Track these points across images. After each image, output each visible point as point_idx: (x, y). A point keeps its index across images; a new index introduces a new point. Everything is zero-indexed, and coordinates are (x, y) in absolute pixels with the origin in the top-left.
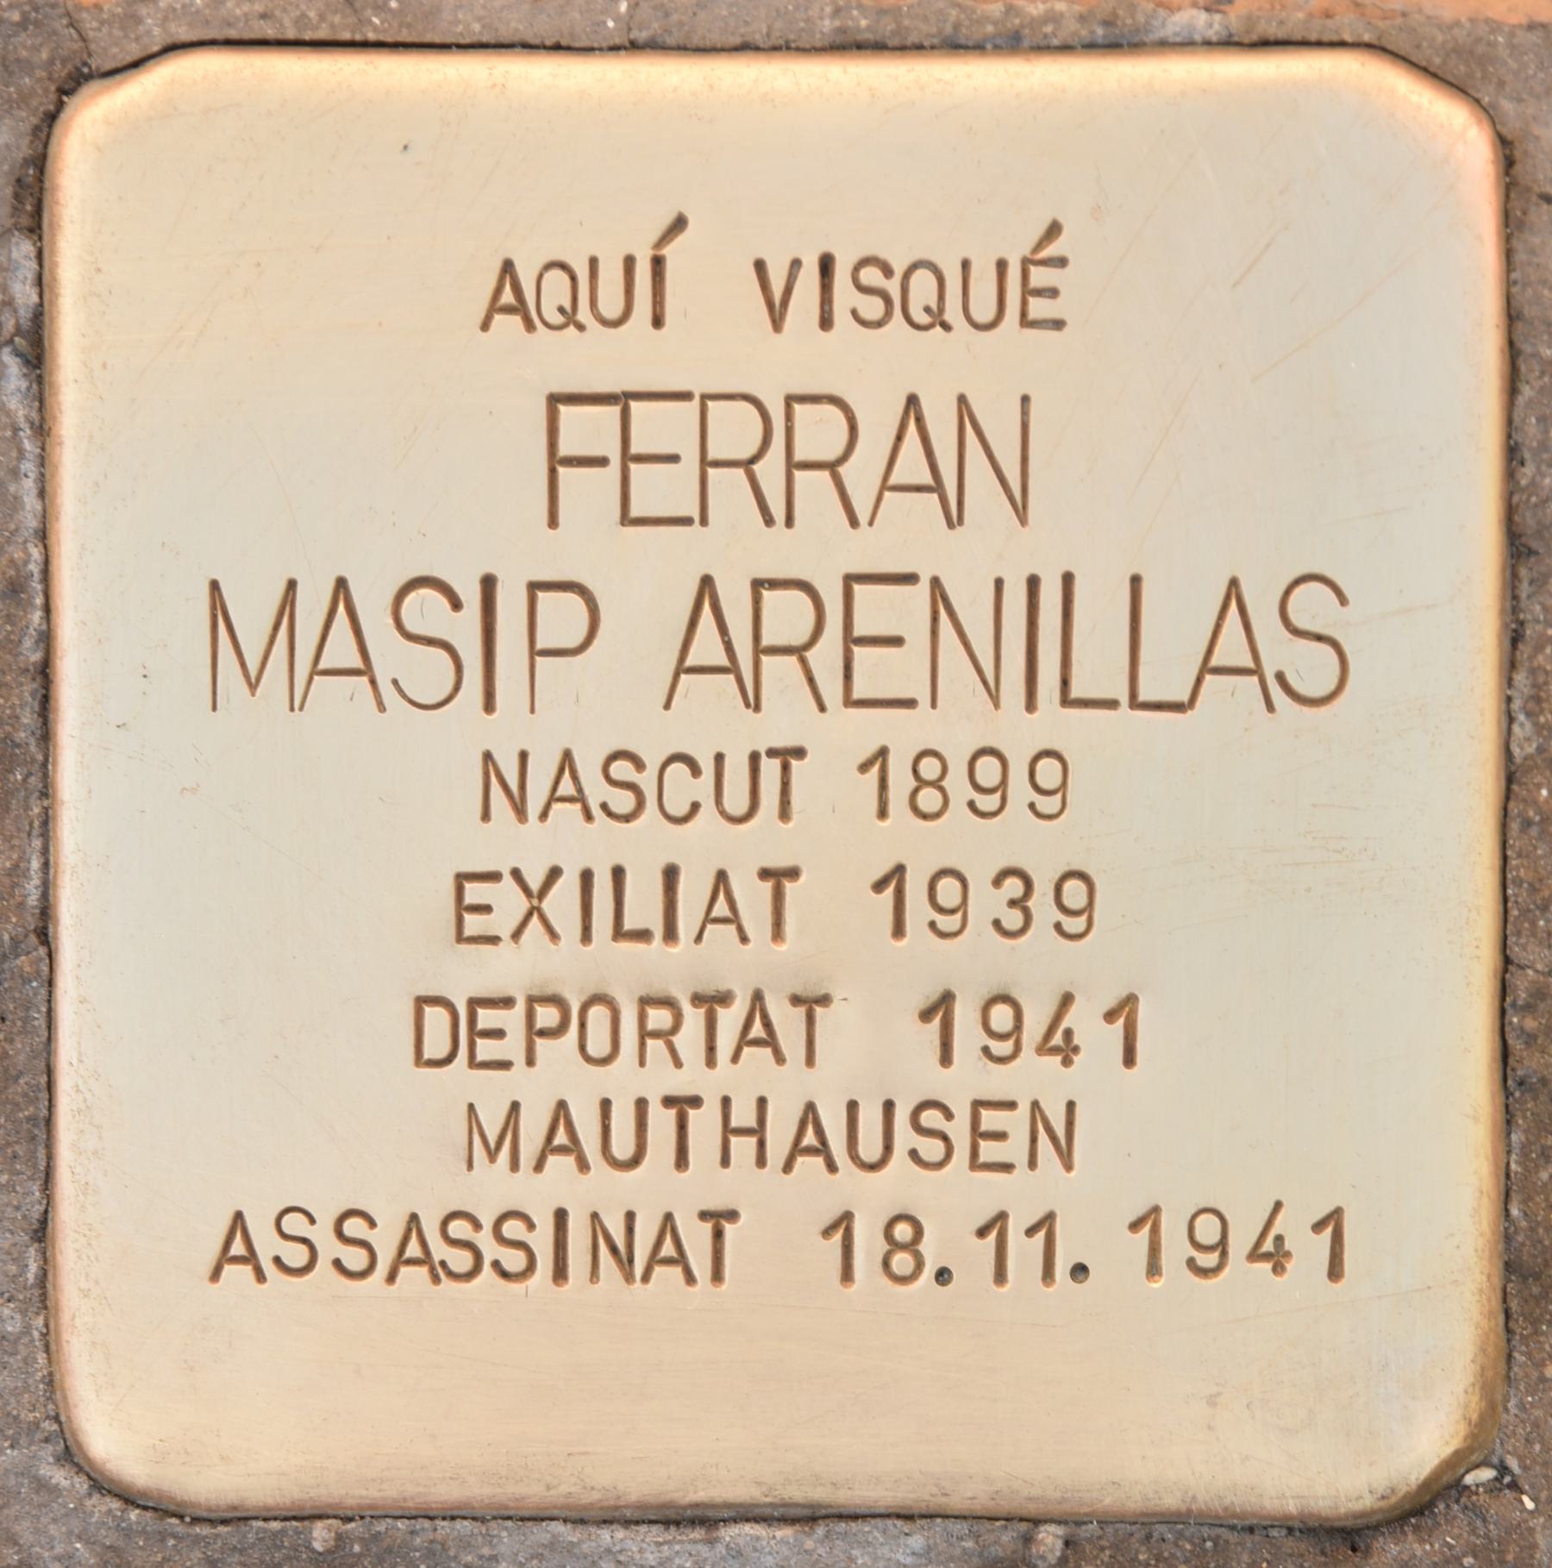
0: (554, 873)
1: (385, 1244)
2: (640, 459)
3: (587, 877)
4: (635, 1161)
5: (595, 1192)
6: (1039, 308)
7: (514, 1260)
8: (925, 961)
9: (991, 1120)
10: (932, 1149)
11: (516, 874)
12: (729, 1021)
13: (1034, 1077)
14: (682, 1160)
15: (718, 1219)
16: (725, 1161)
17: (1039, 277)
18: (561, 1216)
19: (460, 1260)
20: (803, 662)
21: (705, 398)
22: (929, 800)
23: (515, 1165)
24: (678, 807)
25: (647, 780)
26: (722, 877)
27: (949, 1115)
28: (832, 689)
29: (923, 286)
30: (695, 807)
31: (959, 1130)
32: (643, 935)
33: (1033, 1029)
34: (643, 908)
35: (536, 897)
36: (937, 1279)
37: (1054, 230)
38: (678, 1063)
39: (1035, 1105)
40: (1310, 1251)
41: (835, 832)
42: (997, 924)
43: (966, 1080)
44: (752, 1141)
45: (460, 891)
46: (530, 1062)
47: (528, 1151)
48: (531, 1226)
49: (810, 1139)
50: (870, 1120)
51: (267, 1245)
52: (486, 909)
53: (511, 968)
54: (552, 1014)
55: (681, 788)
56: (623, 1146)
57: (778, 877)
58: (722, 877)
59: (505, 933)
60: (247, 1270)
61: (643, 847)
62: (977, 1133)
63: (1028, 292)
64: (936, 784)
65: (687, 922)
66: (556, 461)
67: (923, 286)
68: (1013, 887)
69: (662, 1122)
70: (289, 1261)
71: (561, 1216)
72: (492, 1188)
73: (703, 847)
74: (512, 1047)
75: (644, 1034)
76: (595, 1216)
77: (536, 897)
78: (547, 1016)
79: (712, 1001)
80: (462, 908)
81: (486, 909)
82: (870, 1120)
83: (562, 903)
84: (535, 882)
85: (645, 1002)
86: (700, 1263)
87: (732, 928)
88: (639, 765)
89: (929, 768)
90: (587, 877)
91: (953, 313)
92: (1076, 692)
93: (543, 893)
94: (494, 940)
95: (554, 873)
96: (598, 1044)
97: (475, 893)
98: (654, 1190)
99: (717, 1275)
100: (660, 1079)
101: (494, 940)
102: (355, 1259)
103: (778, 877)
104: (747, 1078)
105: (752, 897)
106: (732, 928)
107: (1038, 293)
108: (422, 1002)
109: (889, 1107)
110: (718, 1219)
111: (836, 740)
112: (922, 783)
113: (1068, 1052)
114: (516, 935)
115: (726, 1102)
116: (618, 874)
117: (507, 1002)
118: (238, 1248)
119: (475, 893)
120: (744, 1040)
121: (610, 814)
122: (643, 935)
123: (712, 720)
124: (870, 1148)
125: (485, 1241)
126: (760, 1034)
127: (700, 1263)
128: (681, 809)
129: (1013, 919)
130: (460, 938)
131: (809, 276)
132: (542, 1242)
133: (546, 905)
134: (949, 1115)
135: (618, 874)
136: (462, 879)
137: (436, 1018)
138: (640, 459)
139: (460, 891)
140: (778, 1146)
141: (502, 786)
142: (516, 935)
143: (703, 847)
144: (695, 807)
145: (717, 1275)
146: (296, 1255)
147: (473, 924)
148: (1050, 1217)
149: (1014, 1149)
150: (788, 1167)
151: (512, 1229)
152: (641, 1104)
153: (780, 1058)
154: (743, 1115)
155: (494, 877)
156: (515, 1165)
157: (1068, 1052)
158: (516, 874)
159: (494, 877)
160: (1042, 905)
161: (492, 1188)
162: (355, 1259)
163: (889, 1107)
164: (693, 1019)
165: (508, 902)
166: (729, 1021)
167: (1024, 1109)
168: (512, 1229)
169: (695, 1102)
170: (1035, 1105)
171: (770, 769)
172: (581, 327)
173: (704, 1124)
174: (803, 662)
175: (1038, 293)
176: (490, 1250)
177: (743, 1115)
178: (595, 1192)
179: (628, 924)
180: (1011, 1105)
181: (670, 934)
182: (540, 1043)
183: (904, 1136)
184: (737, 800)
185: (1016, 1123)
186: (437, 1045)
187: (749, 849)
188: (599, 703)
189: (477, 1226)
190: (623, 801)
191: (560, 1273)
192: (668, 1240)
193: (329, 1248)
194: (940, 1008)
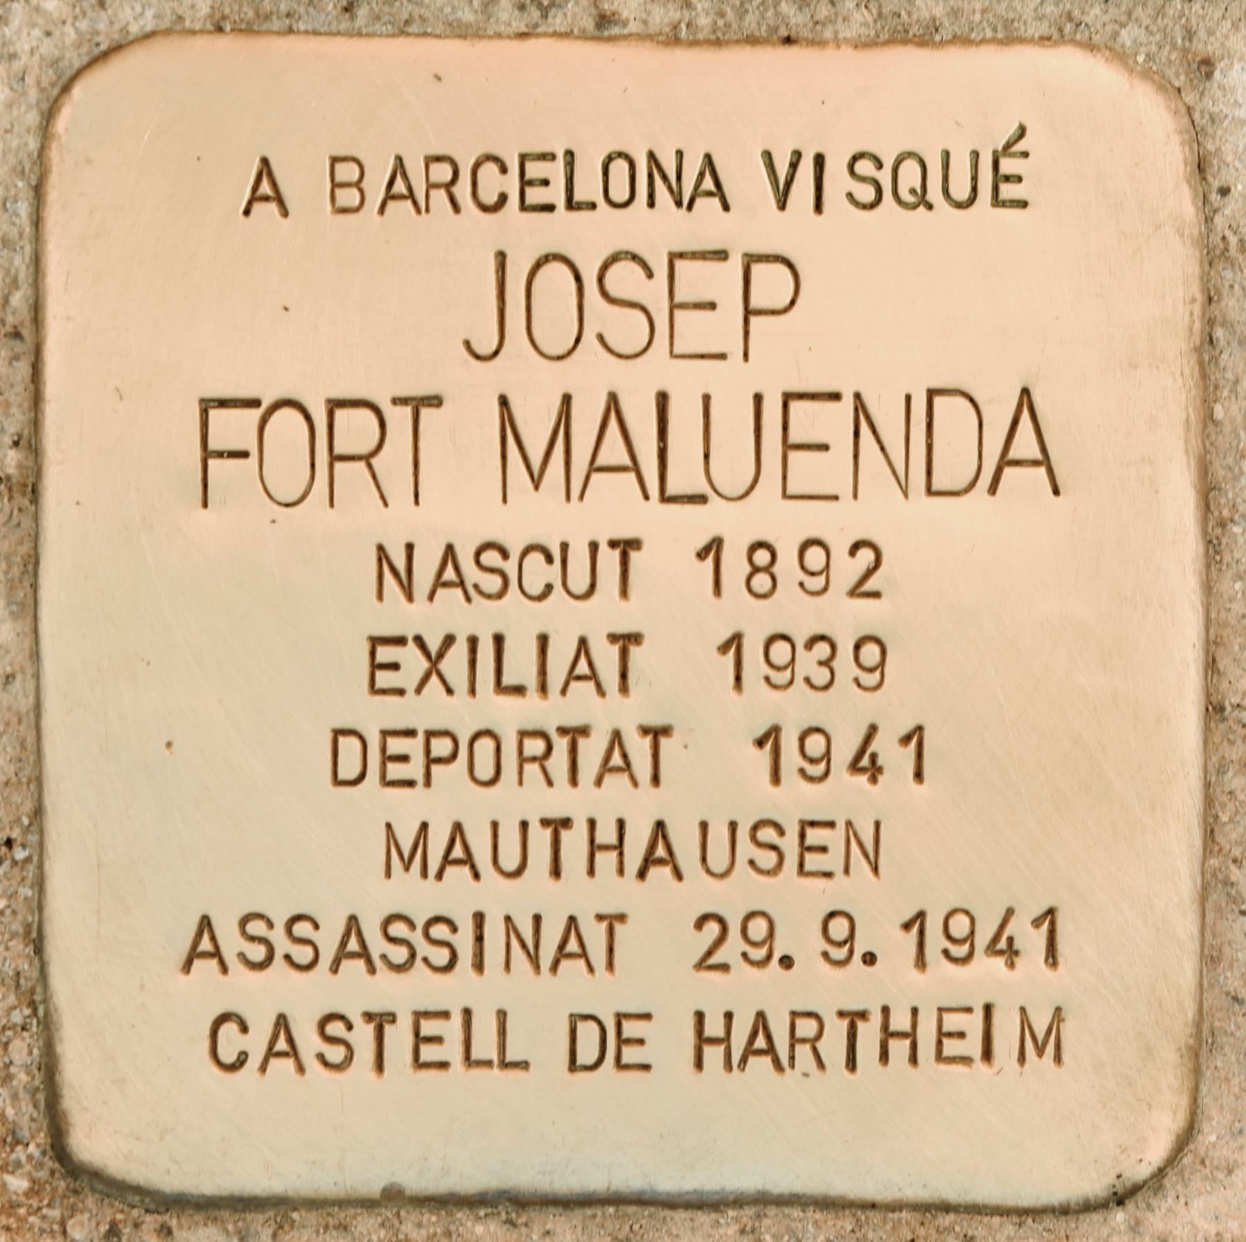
0: (449, 640)
1: (328, 943)
2: (683, 306)
3: (473, 642)
4: (518, 872)
5: (496, 897)
6: (1007, 191)
7: (440, 956)
8: (762, 705)
9: (815, 836)
10: (767, 859)
11: (419, 640)
12: (592, 751)
13: (844, 794)
14: (556, 872)
15: (613, 920)
16: (591, 871)
17: (1007, 166)
18: (479, 919)
19: (399, 954)
20: (370, 466)
21: (751, 260)
22: (762, 582)
23: (424, 874)
24: (536, 588)
25: (511, 567)
26: (583, 642)
27: (781, 832)
28: (653, 489)
29: (910, 175)
30: (549, 588)
31: (790, 844)
32: (519, 690)
33: (843, 752)
34: (520, 667)
35: (434, 661)
36: (865, 962)
37: (1022, 132)
38: (550, 783)
39: (849, 824)
40: (1032, 941)
41: (674, 604)
42: (807, 680)
43: (796, 799)
44: (614, 855)
45: (373, 654)
46: (428, 783)
47: (433, 867)
48: (454, 929)
49: (659, 852)
50: (718, 835)
51: (231, 943)
52: (395, 666)
53: (430, 708)
54: (441, 749)
55: (538, 573)
56: (510, 861)
57: (626, 641)
58: (583, 642)
59: (411, 688)
60: (360, 964)
61: (518, 620)
62: (805, 849)
63: (1000, 178)
64: (767, 569)
65: (557, 675)
66: (207, 454)
67: (910, 172)
68: (822, 650)
69: (540, 839)
70: (297, 959)
71: (479, 919)
72: (418, 896)
73: (566, 621)
74: (414, 769)
75: (523, 760)
76: (508, 919)
77: (434, 661)
78: (441, 747)
79: (576, 733)
80: (375, 666)
81: (395, 666)
82: (718, 835)
83: (455, 664)
84: (434, 647)
85: (523, 734)
86: (598, 954)
87: (591, 684)
88: (505, 555)
89: (762, 557)
90: (473, 642)
91: (934, 194)
92: (790, 491)
93: (441, 655)
94: (401, 692)
95: (449, 640)
96: (485, 770)
97: (385, 654)
98: (537, 896)
99: (610, 965)
100: (560, 801)
101: (401, 692)
102: (303, 954)
103: (626, 641)
104: (634, 804)
105: (606, 658)
106: (591, 684)
107: (1007, 179)
108: (338, 733)
109: (733, 826)
110: (613, 920)
111: (670, 535)
112: (756, 570)
113: (875, 772)
114: (419, 690)
115: (592, 823)
116: (499, 640)
117: (411, 733)
118: (353, 945)
119: (385, 654)
120: (606, 767)
121: (481, 593)
122: (519, 690)
123: (537, 515)
124: (718, 860)
125: (417, 938)
126: (617, 761)
127: (598, 954)
128: (536, 590)
129: (821, 676)
130: (374, 690)
131: (806, 170)
132: (464, 942)
133: (425, 665)
134: (781, 832)
135: (499, 640)
136: (376, 642)
137: (349, 746)
138: (683, 306)
139: (373, 654)
140: (634, 858)
141: (393, 569)
142: (419, 690)
143: (566, 621)
144: (549, 588)
145: (610, 965)
146: (257, 953)
147: (385, 679)
148: (1051, 912)
149: (832, 860)
150: (642, 874)
151: (440, 931)
152: (524, 825)
153: (635, 783)
154: (606, 835)
155: (400, 641)
156: (424, 874)
157: (875, 772)
158: (419, 640)
159: (400, 641)
160: (845, 663)
161: (418, 896)
162: (303, 954)
163: (733, 826)
164: (561, 745)
165: (413, 662)
166: (592, 751)
167: (841, 825)
168: (440, 931)
169: (566, 823)
170: (849, 824)
171: (609, 560)
172: (930, 207)
173: (574, 843)
174: (370, 466)
175: (1007, 179)
176: (282, 944)
177: (606, 835)
178: (496, 897)
179: (507, 680)
180: (831, 825)
181: (543, 688)
182: (435, 769)
183: (745, 848)
184: (579, 581)
185: (834, 838)
186: (349, 769)
187: (604, 615)
188: (463, 498)
189: (270, 925)
190: (492, 583)
191: (479, 966)
192: (206, 937)
193: (282, 944)
194: (769, 738)
